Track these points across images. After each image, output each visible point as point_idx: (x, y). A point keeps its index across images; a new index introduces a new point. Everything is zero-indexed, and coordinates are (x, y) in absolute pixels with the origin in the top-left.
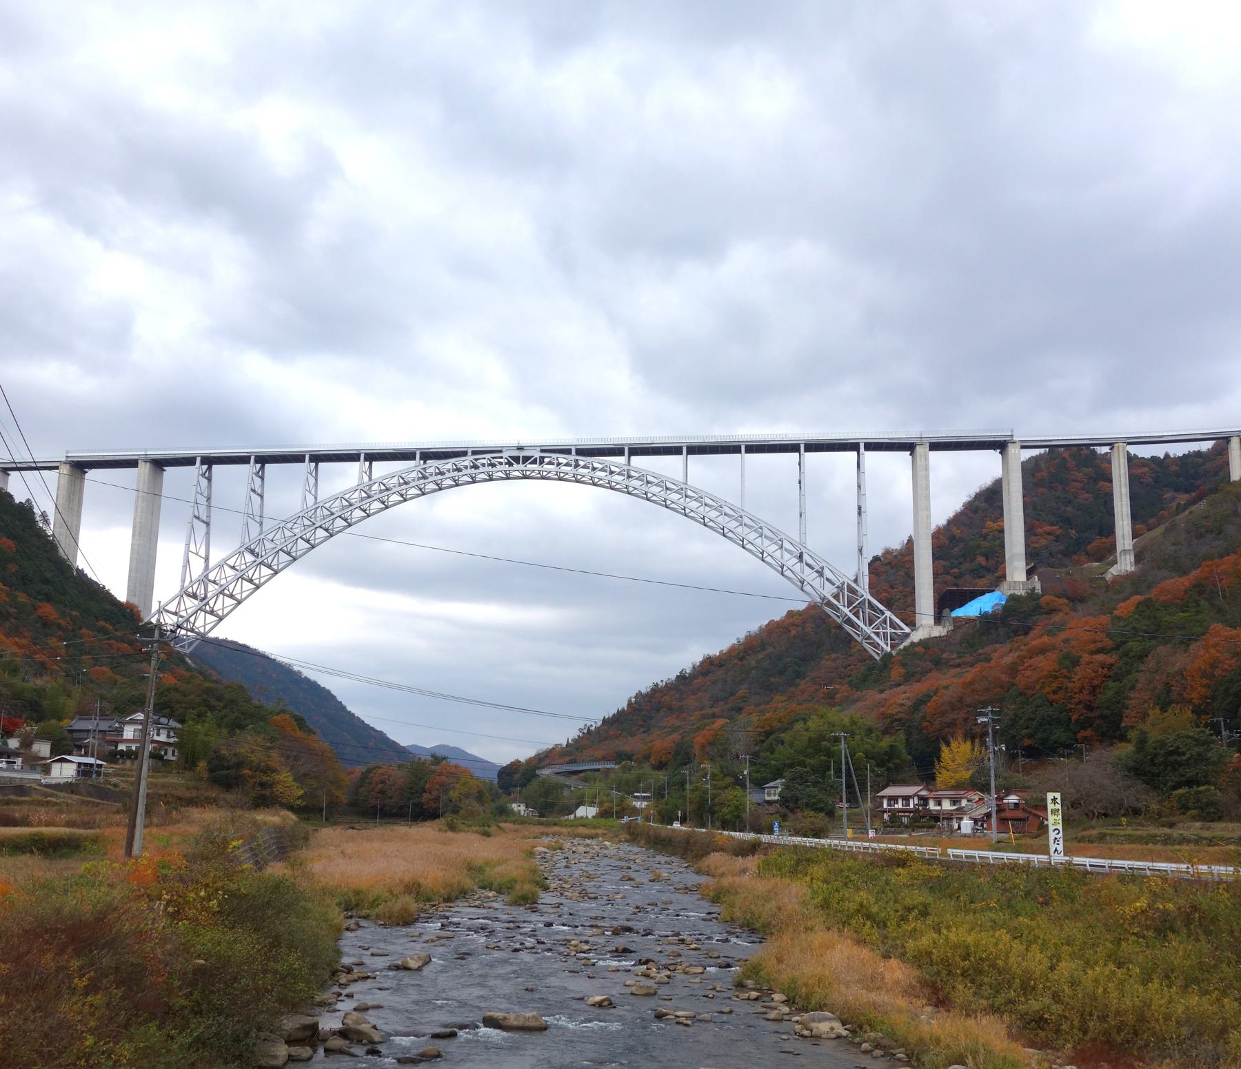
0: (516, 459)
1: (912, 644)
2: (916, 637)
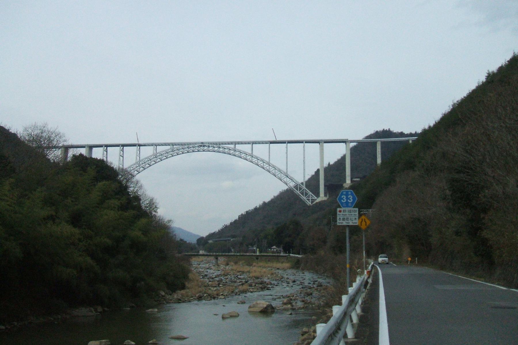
0: (201, 146)
1: (317, 203)
2: (318, 200)
